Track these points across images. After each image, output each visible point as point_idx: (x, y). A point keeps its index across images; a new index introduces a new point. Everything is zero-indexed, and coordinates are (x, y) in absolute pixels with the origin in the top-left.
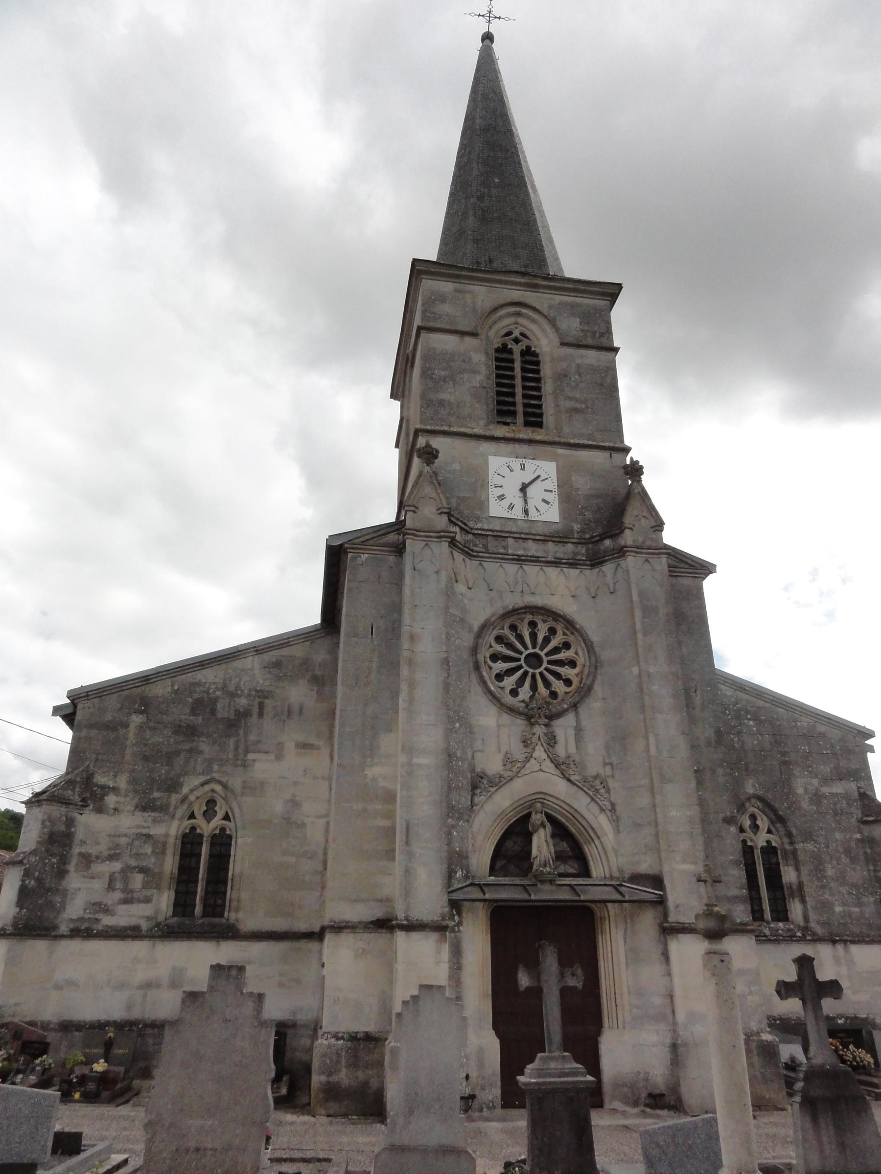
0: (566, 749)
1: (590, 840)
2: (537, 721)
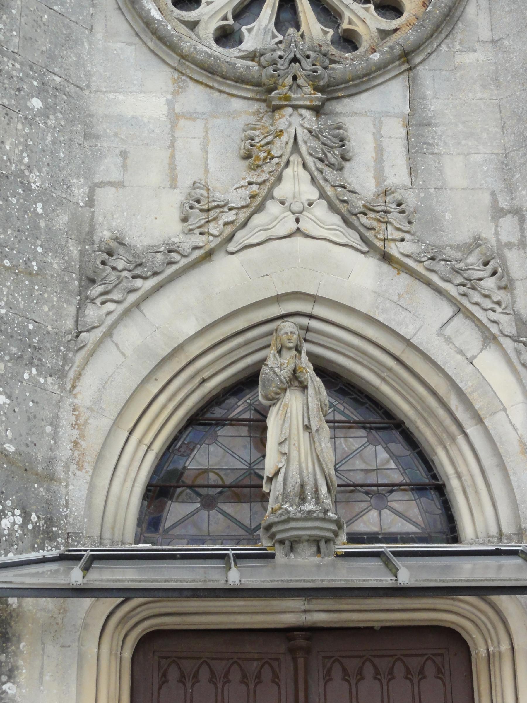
0: (379, 177)
1: (453, 428)
2: (287, 98)
